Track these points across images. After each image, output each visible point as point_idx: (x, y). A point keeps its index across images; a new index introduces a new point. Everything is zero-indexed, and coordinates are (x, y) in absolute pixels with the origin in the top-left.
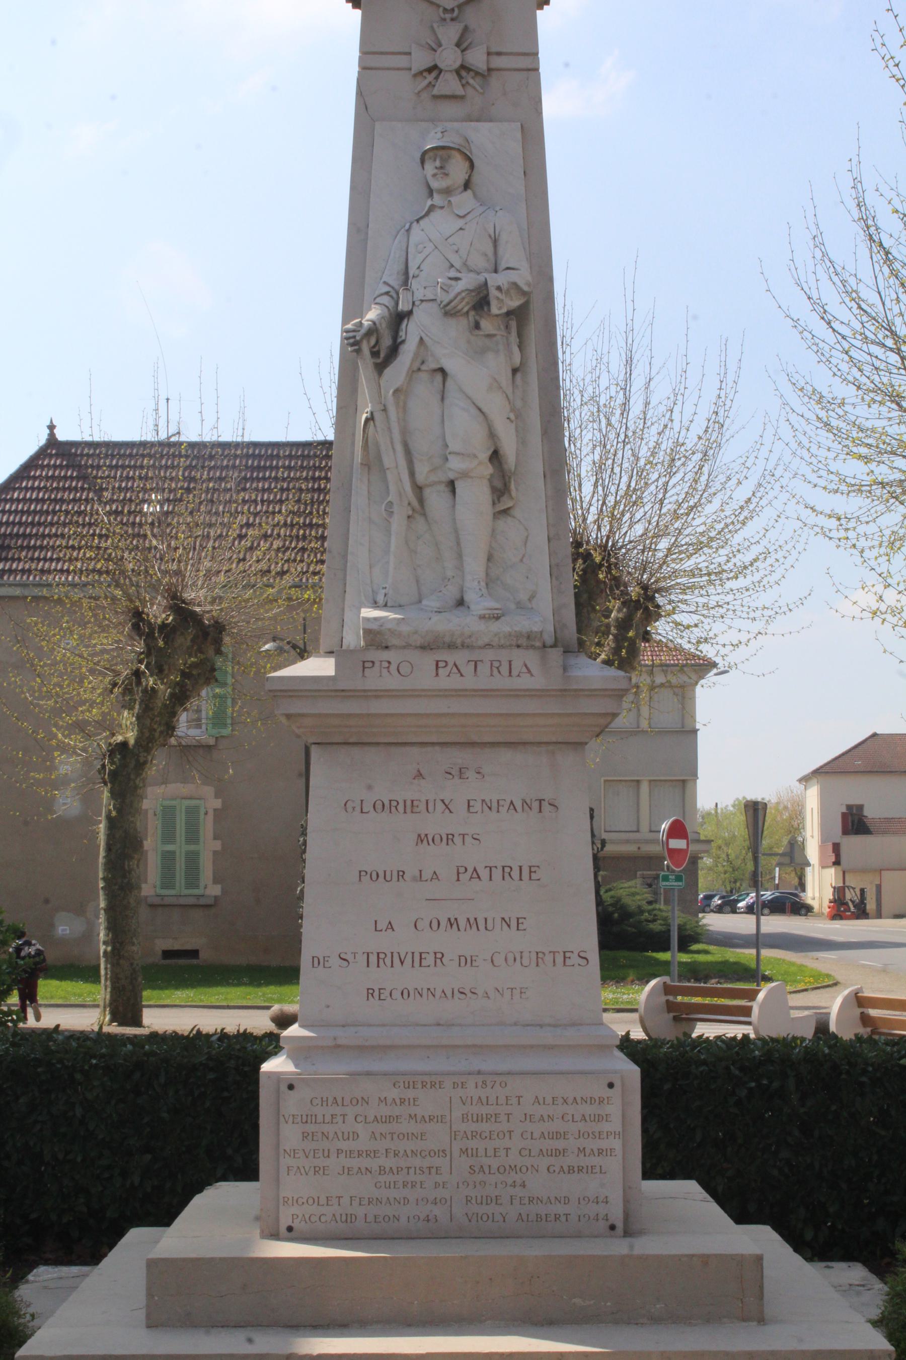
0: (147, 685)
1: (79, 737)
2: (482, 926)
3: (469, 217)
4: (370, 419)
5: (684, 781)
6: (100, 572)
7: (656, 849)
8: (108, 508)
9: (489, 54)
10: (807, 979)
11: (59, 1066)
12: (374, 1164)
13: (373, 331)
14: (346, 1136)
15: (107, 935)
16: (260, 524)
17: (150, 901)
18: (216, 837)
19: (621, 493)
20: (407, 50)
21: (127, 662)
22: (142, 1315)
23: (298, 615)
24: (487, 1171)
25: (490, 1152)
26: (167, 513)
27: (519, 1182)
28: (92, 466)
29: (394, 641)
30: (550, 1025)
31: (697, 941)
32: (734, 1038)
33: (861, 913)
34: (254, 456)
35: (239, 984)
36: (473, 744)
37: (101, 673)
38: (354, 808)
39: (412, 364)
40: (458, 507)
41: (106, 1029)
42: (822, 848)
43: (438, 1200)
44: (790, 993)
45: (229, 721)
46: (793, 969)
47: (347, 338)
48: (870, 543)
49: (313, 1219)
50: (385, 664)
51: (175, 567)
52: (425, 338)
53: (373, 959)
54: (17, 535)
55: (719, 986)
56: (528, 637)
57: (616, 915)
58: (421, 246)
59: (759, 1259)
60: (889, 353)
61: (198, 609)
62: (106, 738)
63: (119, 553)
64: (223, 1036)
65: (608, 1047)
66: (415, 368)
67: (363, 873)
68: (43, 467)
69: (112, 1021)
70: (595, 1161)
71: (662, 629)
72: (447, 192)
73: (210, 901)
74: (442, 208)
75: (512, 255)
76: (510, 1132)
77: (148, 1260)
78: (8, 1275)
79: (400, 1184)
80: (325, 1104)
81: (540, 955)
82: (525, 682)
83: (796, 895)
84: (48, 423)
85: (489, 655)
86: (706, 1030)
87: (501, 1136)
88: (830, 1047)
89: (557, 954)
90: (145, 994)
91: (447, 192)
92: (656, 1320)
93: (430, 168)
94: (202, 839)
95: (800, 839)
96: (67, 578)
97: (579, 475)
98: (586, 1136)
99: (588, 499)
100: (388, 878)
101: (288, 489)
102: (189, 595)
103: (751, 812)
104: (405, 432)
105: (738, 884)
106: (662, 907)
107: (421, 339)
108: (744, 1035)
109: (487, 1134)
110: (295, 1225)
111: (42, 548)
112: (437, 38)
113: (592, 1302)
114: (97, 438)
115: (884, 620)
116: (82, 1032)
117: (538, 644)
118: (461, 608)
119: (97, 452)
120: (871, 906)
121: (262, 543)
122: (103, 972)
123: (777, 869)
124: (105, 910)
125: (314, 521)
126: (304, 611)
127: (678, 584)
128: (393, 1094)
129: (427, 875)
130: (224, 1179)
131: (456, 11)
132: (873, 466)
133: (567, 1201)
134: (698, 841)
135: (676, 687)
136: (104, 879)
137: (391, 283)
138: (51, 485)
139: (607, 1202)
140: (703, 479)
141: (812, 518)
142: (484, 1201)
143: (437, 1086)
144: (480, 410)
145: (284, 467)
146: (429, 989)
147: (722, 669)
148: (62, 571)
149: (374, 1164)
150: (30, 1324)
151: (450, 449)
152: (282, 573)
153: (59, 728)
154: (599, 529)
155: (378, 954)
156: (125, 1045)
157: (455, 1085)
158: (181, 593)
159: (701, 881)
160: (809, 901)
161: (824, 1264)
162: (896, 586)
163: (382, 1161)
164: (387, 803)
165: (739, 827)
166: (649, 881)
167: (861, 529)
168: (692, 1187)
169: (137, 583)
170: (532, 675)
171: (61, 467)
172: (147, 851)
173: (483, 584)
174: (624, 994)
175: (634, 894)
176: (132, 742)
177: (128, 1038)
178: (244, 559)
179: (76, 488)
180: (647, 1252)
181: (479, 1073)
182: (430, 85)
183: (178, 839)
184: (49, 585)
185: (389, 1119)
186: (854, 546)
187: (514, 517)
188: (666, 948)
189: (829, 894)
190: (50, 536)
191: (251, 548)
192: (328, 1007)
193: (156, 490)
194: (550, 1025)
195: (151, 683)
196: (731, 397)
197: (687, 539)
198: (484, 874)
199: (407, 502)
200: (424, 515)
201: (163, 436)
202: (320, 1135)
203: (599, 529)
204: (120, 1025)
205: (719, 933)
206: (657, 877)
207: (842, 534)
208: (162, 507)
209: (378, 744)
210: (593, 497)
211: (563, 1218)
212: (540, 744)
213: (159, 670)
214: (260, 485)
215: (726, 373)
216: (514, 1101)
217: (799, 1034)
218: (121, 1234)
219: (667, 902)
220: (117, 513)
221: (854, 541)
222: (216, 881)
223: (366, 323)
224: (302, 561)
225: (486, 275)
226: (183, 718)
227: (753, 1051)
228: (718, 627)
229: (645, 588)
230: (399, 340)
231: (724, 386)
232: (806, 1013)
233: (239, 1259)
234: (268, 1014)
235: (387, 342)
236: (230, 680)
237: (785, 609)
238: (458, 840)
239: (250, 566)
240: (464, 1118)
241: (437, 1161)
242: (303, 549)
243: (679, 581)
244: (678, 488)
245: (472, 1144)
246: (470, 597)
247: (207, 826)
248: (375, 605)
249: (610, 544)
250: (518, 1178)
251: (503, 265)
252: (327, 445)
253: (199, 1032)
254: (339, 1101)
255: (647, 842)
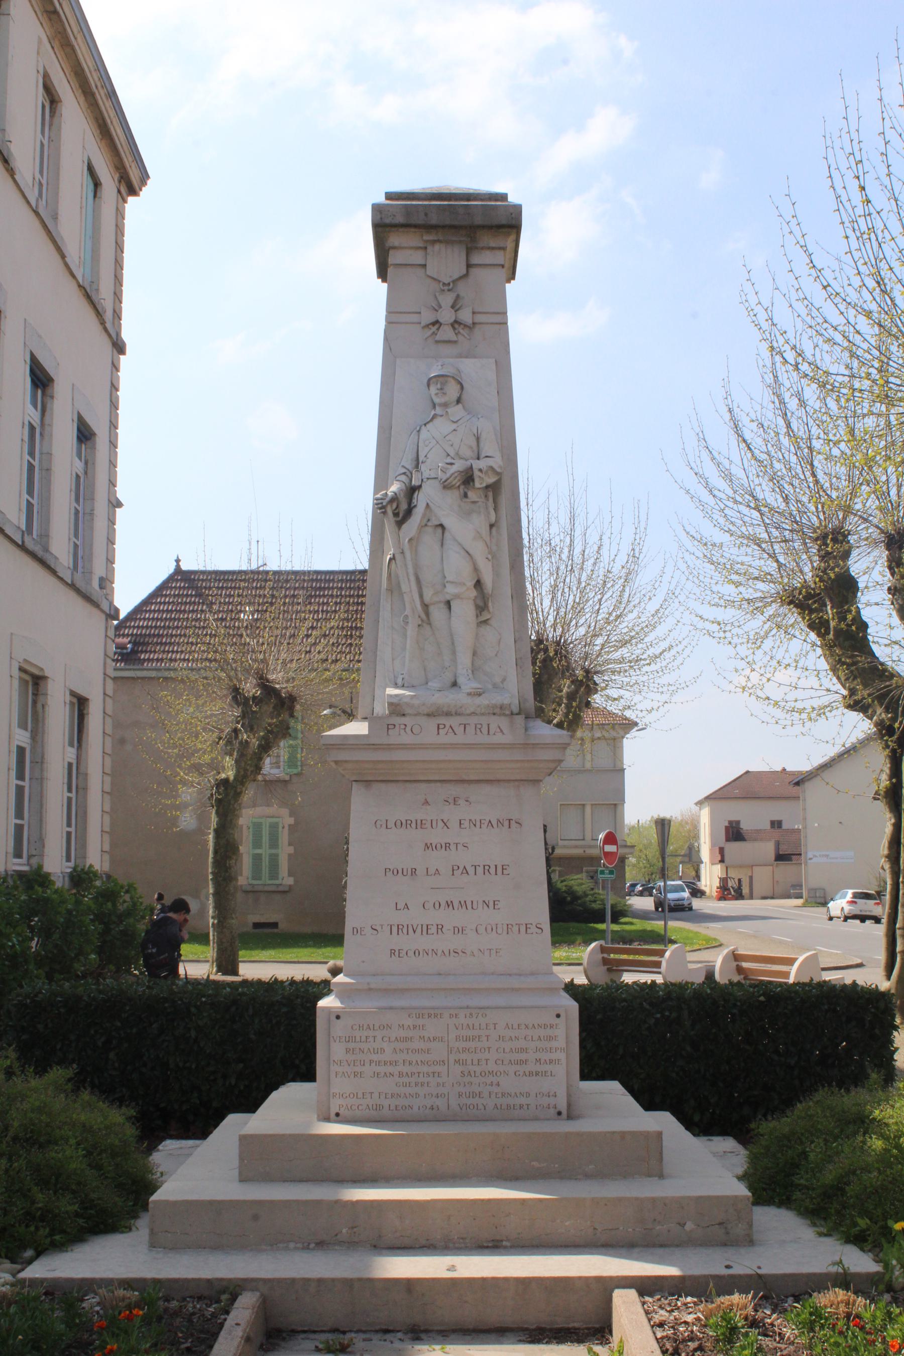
0: (242, 739)
1: (195, 775)
2: (469, 906)
3: (460, 422)
4: (393, 559)
5: (615, 805)
6: (210, 661)
7: (595, 852)
8: (216, 616)
9: (474, 313)
10: (700, 942)
11: (179, 1002)
12: (395, 1070)
13: (395, 499)
14: (376, 1051)
15: (214, 912)
16: (321, 627)
17: (244, 888)
18: (290, 844)
19: (569, 607)
20: (419, 311)
21: (228, 723)
22: (236, 1173)
23: (346, 691)
24: (473, 1075)
25: (475, 1062)
26: (257, 620)
27: (495, 1082)
28: (205, 588)
29: (408, 711)
30: (516, 974)
31: (625, 916)
32: (646, 983)
33: (739, 896)
34: (317, 580)
35: (306, 946)
36: (463, 781)
37: (210, 730)
38: (381, 825)
39: (421, 521)
40: (453, 618)
41: (212, 977)
42: (711, 850)
43: (439, 1095)
44: (689, 951)
45: (299, 763)
46: (691, 935)
47: (377, 504)
48: (741, 641)
49: (353, 1107)
50: (403, 727)
51: (261, 657)
52: (430, 504)
53: (395, 929)
54: (154, 635)
55: (639, 947)
56: (501, 708)
57: (569, 899)
58: (428, 442)
59: (659, 1135)
60: (752, 511)
61: (277, 686)
62: (214, 775)
63: (224, 647)
64: (293, 982)
65: (556, 989)
66: (423, 524)
67: (387, 870)
68: (171, 588)
69: (218, 971)
70: (547, 1067)
71: (597, 699)
72: (445, 405)
73: (287, 889)
74: (442, 416)
75: (489, 447)
76: (489, 1048)
77: (240, 1135)
78: (145, 1145)
79: (413, 1084)
80: (361, 1029)
81: (510, 926)
82: (498, 739)
83: (694, 884)
84: (176, 558)
85: (473, 720)
86: (628, 978)
87: (483, 1050)
88: (711, 989)
89: (521, 926)
90: (241, 953)
91: (445, 405)
92: (588, 1176)
93: (433, 390)
94: (280, 846)
95: (696, 844)
96: (188, 665)
97: (541, 594)
98: (541, 1050)
99: (546, 610)
100: (405, 873)
101: (340, 603)
102: (271, 677)
103: (659, 827)
104: (416, 567)
105: (654, 876)
106: (601, 892)
107: (428, 504)
108: (652, 980)
109: (473, 1050)
110: (341, 1112)
111: (170, 644)
112: (439, 303)
113: (545, 1165)
114: (209, 568)
115: (751, 694)
116: (196, 979)
117: (508, 712)
118: (455, 688)
119: (209, 578)
120: (745, 891)
121: (322, 640)
122: (211, 938)
123: (681, 865)
124: (213, 894)
125: (358, 625)
126: (350, 688)
127: (610, 669)
128: (409, 1022)
129: (432, 871)
130: (294, 1080)
131: (451, 284)
132: (741, 589)
133: (528, 1095)
134: (626, 846)
135: (609, 739)
136: (212, 873)
137: (407, 467)
138: (177, 601)
139: (556, 1096)
140: (626, 594)
141: (701, 624)
142: (471, 1096)
143: (439, 1016)
144: (467, 552)
145: (337, 588)
146: (433, 950)
147: (641, 727)
148: (184, 660)
149: (395, 1070)
150: (160, 1180)
151: (448, 579)
152: (336, 661)
153: (181, 768)
154: (555, 630)
155: (398, 926)
156: (225, 989)
157: (451, 1016)
158: (266, 675)
159: (628, 875)
160: (703, 888)
161: (706, 1138)
162: (758, 670)
163: (401, 1068)
164: (404, 822)
165: (653, 835)
166: (592, 874)
167: (735, 631)
168: (615, 1085)
169: (236, 668)
170: (503, 734)
171: (184, 588)
172: (242, 854)
173: (470, 671)
174: (573, 953)
175: (582, 884)
176: (232, 778)
177: (227, 983)
178: (310, 652)
179: (194, 603)
180: (583, 1130)
181: (468, 1007)
182: (434, 334)
183: (264, 846)
184: (175, 670)
185: (406, 1039)
186: (730, 643)
187: (491, 626)
188: (603, 921)
189: (717, 883)
190: (176, 636)
191: (315, 644)
192: (363, 962)
193: (249, 604)
194: (516, 974)
195: (245, 737)
196: (643, 539)
197: (616, 638)
198: (471, 870)
199: (417, 617)
200: (430, 624)
201: (254, 567)
202: (358, 1050)
203: (555, 630)
204: (224, 974)
205: (641, 910)
206: (596, 872)
207: (722, 634)
208: (253, 615)
209: (397, 781)
210: (550, 608)
211: (525, 1107)
212: (509, 781)
213: (251, 728)
214: (321, 600)
215: (639, 523)
216: (492, 1027)
217: (690, 980)
218: (222, 1118)
219: (603, 888)
220: (222, 620)
221: (730, 639)
222: (290, 875)
223: (390, 494)
224: (350, 652)
225: (472, 461)
226: (267, 761)
227: (658, 992)
228: (637, 698)
229: (587, 672)
230: (413, 505)
231: (638, 532)
232: (699, 965)
233: (302, 1135)
234: (327, 966)
235: (404, 506)
236: (300, 735)
237: (683, 685)
238: (453, 847)
239: (314, 656)
240: (457, 1038)
241: (438, 1068)
242: (351, 645)
243: (610, 666)
244: (609, 602)
245: (463, 1056)
246: (461, 680)
247: (284, 837)
248: (396, 686)
249: (562, 641)
250: (494, 1079)
251: (483, 455)
252: (363, 572)
253: (276, 979)
254: (371, 1027)
255: (590, 847)
